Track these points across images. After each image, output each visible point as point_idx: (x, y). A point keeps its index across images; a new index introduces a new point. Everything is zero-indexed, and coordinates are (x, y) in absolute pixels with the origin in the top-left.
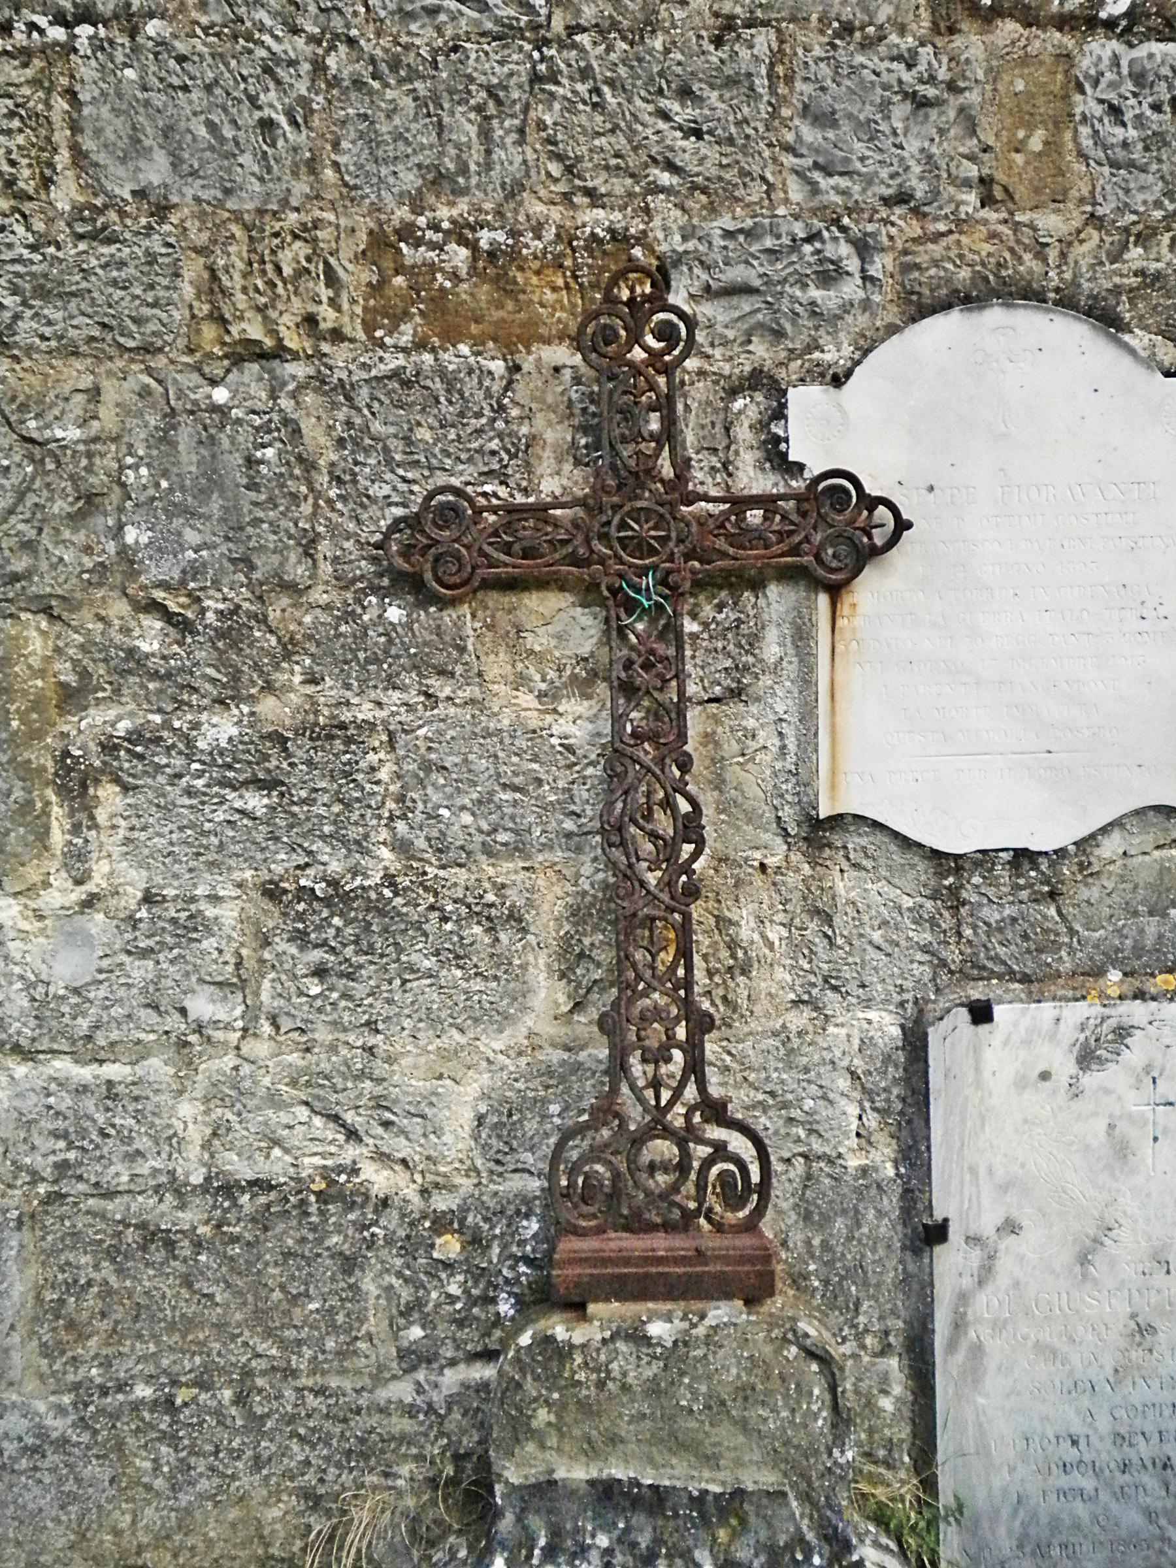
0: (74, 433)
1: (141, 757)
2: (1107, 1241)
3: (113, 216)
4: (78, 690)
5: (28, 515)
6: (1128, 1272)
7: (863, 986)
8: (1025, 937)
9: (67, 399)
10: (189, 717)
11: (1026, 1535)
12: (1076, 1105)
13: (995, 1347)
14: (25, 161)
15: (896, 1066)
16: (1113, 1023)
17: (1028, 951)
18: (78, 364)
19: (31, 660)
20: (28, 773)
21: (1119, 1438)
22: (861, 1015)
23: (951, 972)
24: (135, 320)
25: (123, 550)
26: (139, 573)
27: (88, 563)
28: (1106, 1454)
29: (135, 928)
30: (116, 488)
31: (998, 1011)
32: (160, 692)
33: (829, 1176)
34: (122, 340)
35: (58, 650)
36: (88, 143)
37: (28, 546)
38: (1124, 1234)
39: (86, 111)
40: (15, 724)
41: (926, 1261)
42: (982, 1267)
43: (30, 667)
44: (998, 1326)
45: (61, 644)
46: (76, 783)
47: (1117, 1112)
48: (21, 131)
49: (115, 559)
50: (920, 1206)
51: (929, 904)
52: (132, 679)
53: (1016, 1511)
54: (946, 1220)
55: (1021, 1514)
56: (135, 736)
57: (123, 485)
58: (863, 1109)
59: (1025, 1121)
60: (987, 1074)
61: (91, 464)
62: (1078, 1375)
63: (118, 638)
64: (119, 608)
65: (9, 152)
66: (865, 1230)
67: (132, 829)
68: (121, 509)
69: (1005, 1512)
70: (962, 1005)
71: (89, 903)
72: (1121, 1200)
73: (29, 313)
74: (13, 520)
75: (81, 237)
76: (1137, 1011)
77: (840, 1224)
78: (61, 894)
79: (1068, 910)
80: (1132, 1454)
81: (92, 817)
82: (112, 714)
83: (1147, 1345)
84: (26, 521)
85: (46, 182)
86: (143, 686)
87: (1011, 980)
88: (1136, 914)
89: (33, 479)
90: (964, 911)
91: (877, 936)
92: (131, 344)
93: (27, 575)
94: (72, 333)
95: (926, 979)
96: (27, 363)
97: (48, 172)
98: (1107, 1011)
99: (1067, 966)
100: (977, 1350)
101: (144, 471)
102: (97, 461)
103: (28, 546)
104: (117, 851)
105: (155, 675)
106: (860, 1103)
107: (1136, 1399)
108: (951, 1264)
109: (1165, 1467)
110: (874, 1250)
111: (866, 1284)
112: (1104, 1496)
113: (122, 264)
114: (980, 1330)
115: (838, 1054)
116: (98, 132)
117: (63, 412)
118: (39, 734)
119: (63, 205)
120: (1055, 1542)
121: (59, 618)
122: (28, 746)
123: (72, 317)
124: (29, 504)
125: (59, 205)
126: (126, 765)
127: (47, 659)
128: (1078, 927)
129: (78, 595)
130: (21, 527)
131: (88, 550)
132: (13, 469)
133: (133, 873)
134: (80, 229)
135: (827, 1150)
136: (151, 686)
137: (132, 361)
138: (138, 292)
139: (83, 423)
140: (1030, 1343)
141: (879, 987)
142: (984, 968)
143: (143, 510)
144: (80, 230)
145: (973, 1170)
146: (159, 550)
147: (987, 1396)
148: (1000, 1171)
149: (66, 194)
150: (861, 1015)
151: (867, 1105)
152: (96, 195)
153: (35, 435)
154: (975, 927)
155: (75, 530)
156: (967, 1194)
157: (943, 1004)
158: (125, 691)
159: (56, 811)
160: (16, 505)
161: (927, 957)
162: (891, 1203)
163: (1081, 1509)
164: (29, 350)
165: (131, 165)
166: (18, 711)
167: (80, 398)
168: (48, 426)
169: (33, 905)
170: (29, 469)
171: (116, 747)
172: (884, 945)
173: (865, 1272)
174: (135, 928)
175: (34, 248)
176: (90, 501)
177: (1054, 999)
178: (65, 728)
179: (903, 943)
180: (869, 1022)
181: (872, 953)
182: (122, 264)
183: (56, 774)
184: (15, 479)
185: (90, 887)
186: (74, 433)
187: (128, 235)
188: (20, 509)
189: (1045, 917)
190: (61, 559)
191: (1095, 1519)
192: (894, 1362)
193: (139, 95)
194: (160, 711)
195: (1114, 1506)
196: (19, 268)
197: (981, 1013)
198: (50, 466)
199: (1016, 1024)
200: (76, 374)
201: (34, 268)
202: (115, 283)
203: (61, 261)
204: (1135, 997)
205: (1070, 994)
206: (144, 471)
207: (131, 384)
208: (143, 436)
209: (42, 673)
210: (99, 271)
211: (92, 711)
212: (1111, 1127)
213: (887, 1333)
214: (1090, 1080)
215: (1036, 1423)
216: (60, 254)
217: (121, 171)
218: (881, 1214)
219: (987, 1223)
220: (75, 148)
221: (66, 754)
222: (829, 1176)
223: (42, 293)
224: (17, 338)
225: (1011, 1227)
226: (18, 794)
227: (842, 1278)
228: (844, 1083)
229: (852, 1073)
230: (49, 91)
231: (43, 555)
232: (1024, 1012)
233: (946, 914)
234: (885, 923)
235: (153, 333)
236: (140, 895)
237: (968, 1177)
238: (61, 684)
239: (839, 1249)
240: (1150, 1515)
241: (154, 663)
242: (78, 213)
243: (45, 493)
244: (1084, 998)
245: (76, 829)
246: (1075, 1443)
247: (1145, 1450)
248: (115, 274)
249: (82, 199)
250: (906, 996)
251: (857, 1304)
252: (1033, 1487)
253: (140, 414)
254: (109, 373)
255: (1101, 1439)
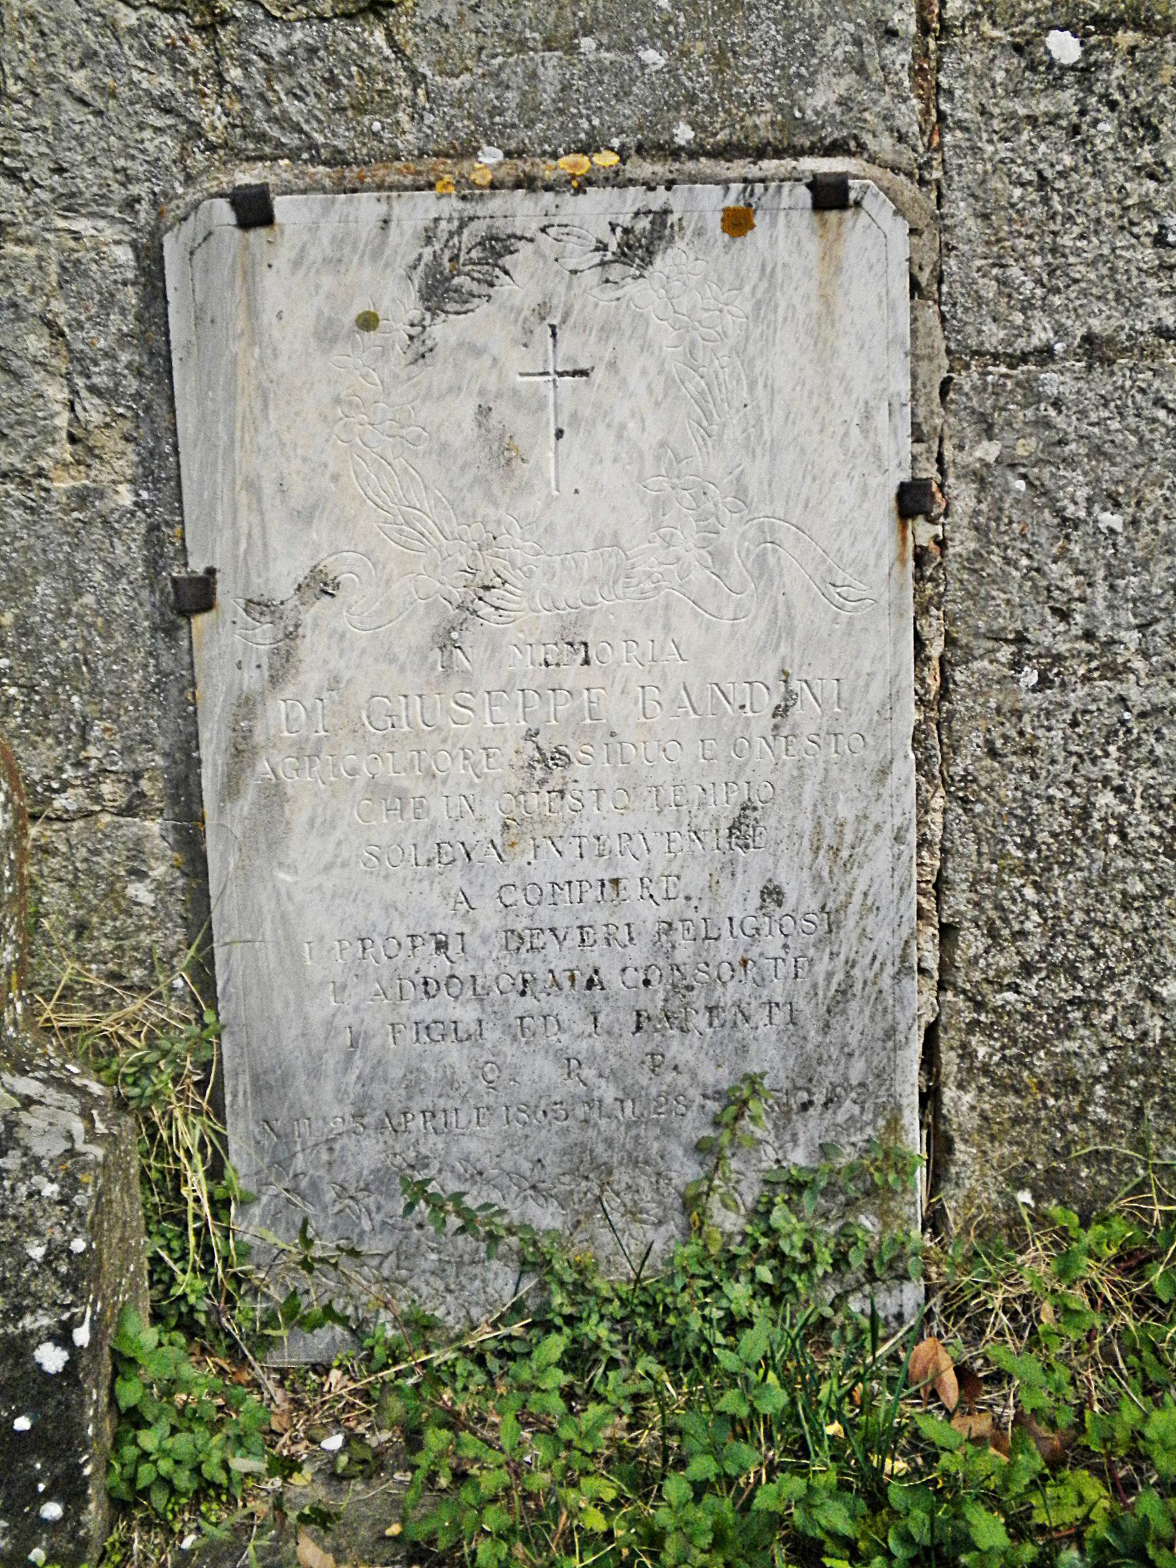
2: (485, 610)
6: (522, 662)
7: (60, 170)
8: (332, 82)
11: (366, 1098)
12: (424, 374)
13: (305, 788)
15: (123, 311)
16: (478, 229)
17: (341, 110)
21: (515, 940)
22: (61, 223)
23: (212, 148)
28: (496, 966)
31: (281, 205)
33: (20, 504)
38: (511, 598)
41: (185, 643)
42: (275, 652)
44: (307, 752)
47: (492, 384)
50: (169, 550)
51: (165, 22)
53: (349, 1057)
54: (211, 572)
55: (358, 1062)
58: (75, 392)
59: (337, 401)
60: (267, 317)
62: (442, 834)
66: (89, 599)
69: (331, 1062)
70: (221, 195)
72: (504, 539)
76: (522, 211)
77: (44, 589)
79: (405, 37)
80: (536, 965)
83: (555, 782)
87: (312, 161)
88: (522, 45)
90: (226, 35)
91: (79, 80)
95: (166, 160)
98: (469, 209)
99: (410, 139)
100: (274, 794)
106: (68, 376)
107: (541, 874)
108: (224, 645)
109: (590, 984)
110: (107, 637)
111: (95, 692)
112: (492, 1035)
114: (277, 758)
115: (23, 290)
120: (416, 1107)
128: (424, 68)
135: (16, 461)
140: (361, 781)
141: (87, 172)
142: (262, 137)
145: (253, 487)
147: (293, 869)
148: (297, 489)
150: (61, 223)
151: (80, 382)
154: (245, 64)
156: (244, 529)
157: (192, 195)
161: (170, 120)
162: (129, 551)
163: (454, 1054)
172: (90, 96)
173: (93, 671)
177: (380, 187)
179: (125, 93)
180: (77, 236)
181: (71, 110)
189: (363, 45)
191: (478, 1071)
192: (154, 826)
195: (508, 1048)
197: (254, 211)
199: (314, 228)
204: (518, 185)
205: (408, 180)
212: (484, 411)
213: (137, 776)
214: (446, 330)
215: (376, 914)
218: (116, 574)
219: (282, 578)
222: (20, 504)
225: (321, 585)
227: (57, 682)
228: (36, 343)
229: (50, 324)
232: (327, 209)
233: (195, 39)
234: (89, 56)
237: (243, 498)
239: (48, 630)
240: (569, 1063)
244: (431, 186)
246: (441, 946)
247: (559, 958)
250: (135, 189)
251: (85, 728)
252: (375, 1021)
255: (485, 940)
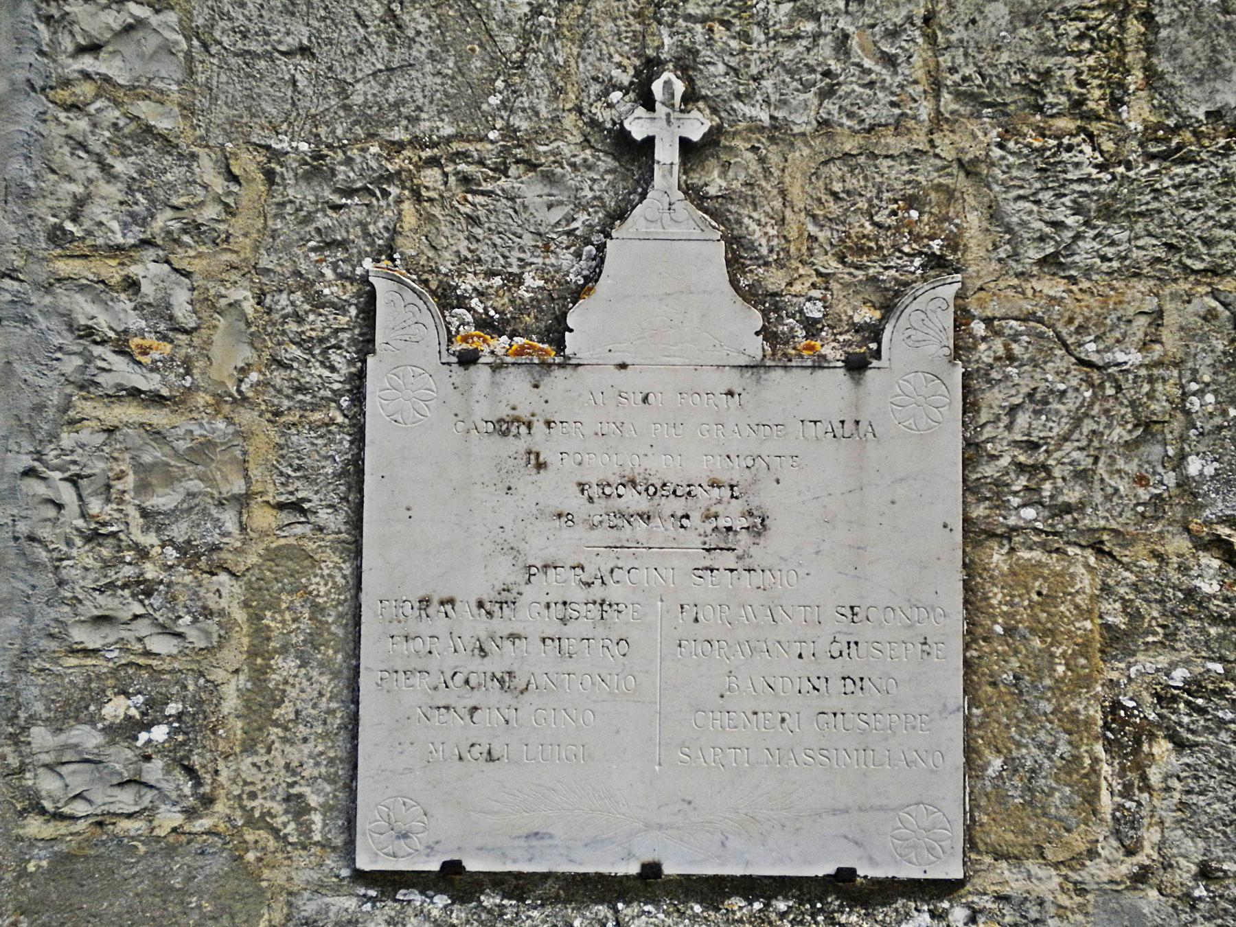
0: (1135, 357)
1: (1202, 711)
3: (1187, 135)
4: (1125, 633)
5: (1084, 443)
9: (1129, 321)
10: (609, 915)
14: (1096, 82)
18: (1141, 286)
19: (1078, 599)
20: (1074, 724)
24: (1207, 242)
25: (1184, 483)
26: (1203, 507)
27: (1144, 495)
29: (1193, 908)
30: (1179, 415)
32: (1222, 638)
34: (1189, 262)
35: (1106, 589)
36: (1162, 64)
37: (1082, 476)
39: (1163, 33)
40: (1060, 669)
43: (1077, 607)
45: (1111, 582)
46: (1125, 734)
48: (1090, 52)
49: (1174, 491)
52: (1191, 623)
56: (1194, 686)
57: (1188, 413)
61: (1153, 390)
63: (1175, 577)
64: (1178, 544)
65: (1079, 73)
67: (1188, 792)
68: (1183, 438)
71: (1141, 877)
73: (1092, 233)
74: (1068, 446)
75: (1153, 157)
78: (1110, 866)
81: (1144, 778)
82: (1163, 661)
84: (1080, 449)
85: (1116, 103)
86: (1202, 631)
89: (1091, 404)
92: (1198, 266)
93: (1081, 506)
94: (1136, 254)
96: (1085, 284)
97: (1118, 93)
101: (1210, 398)
102: (1159, 386)
103: (1082, 476)
104: (1169, 818)
105: (1217, 619)
113: (1197, 184)
116: (1174, 54)
117: (1124, 335)
118: (1085, 682)
119: (1135, 125)
121: (1110, 554)
122: (1074, 694)
123: (1137, 238)
124: (1085, 431)
125: (1132, 125)
126: (1186, 720)
127: (1094, 599)
129: (1131, 529)
130: (1076, 455)
131: (1141, 480)
132: (1070, 394)
133: (1188, 842)
134: (1153, 149)
136: (1213, 631)
137: (1198, 283)
138: (1212, 212)
139: (1144, 346)
143: (1207, 440)
144: (1155, 150)
146: (1228, 482)
149: (1137, 114)
152: (1168, 115)
153: (1094, 358)
155: (1128, 460)
158: (1182, 636)
159: (1106, 769)
160: (1071, 431)
164: (1088, 272)
165: (1208, 86)
166: (1063, 655)
167: (1143, 321)
168: (1108, 349)
169: (1074, 876)
170: (1088, 394)
171: (1175, 699)
174: (1193, 908)
175: (1101, 167)
176: (1148, 427)
178: (1114, 675)
182: (1197, 184)
183: (1106, 726)
184: (1071, 403)
185: (1141, 858)
186: (1135, 357)
187: (1204, 155)
188: (1076, 436)
190: (1116, 490)
193: (1221, 18)
194: (1222, 659)
196: (1085, 187)
198: (1110, 391)
200: (1139, 296)
201: (1103, 188)
202: (1187, 203)
203: (1132, 181)
206: (1210, 398)
207: (1196, 306)
208: (1209, 361)
209: (1087, 614)
210: (1172, 191)
211: (1140, 657)
216: (1131, 174)
217: (1196, 92)
220: (1149, 70)
221: (1116, 705)
223: (1108, 214)
224: (1077, 258)
226: (1063, 748)
230: (1123, 15)
231: (1097, 485)
235: (1225, 255)
236: (1194, 869)
238: (1107, 627)
241: (1215, 605)
242: (1150, 132)
243: (1104, 420)
245: (1127, 792)
248: (1189, 194)
249: (1153, 119)
253: (1204, 338)
254: (1174, 296)
